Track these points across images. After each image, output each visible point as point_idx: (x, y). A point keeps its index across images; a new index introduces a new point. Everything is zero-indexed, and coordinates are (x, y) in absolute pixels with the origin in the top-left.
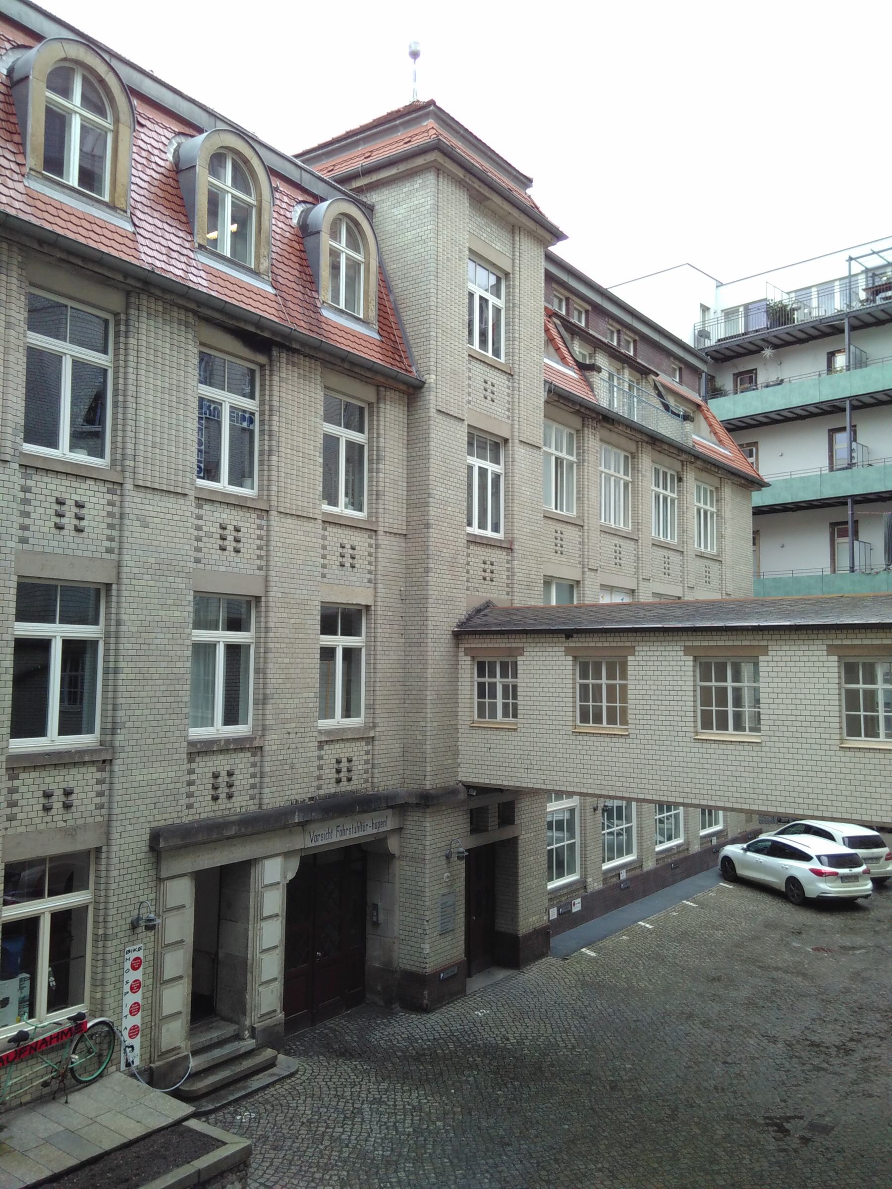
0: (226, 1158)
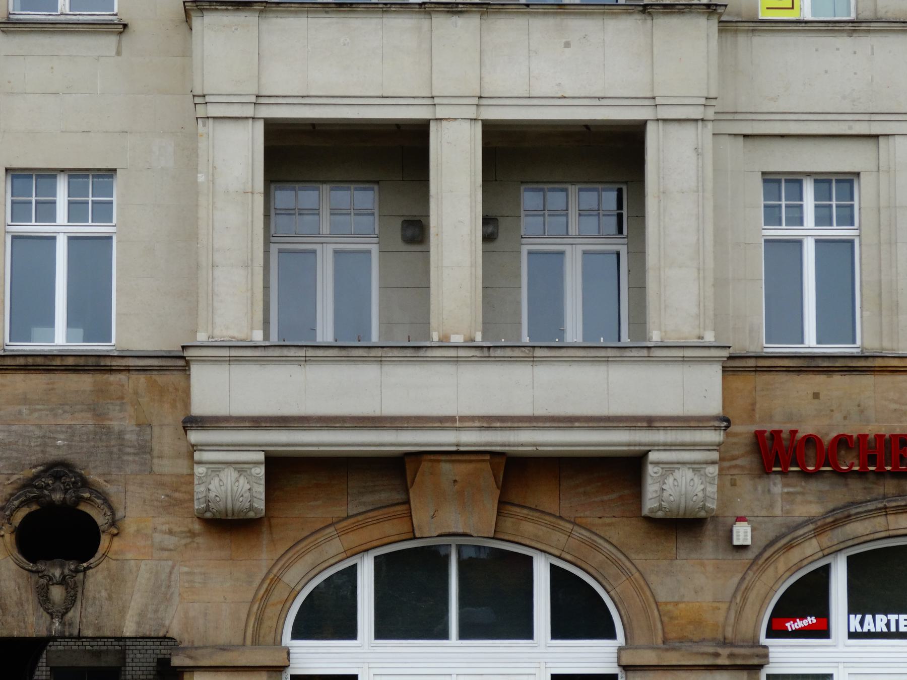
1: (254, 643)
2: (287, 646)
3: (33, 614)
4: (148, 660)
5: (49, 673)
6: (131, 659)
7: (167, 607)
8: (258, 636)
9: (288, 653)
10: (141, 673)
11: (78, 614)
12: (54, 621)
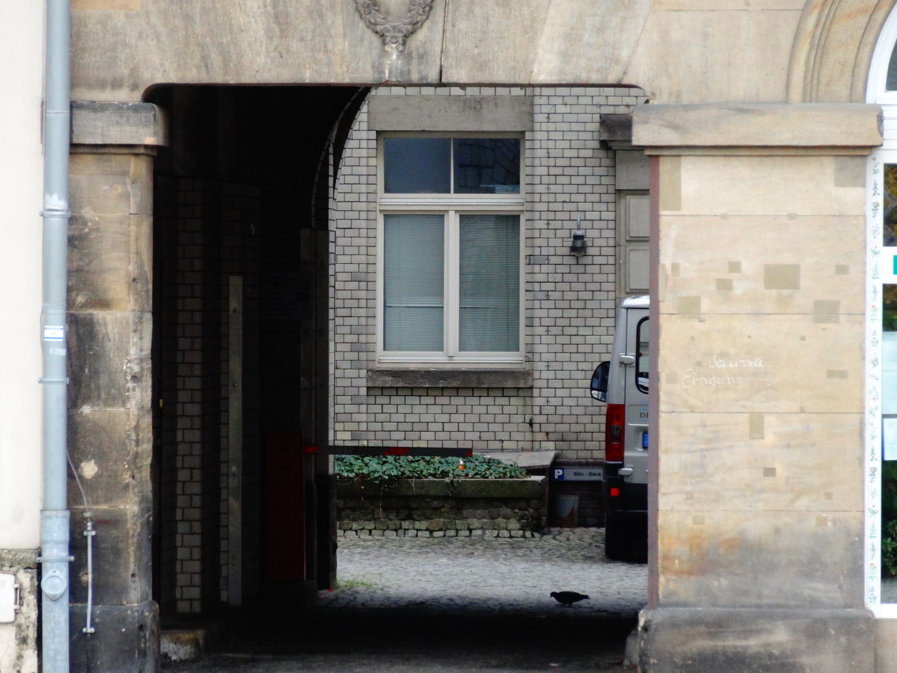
1: (808, 99)
2: (878, 102)
3: (344, 35)
4: (582, 118)
5: (373, 144)
6: (547, 115)
7: (624, 20)
8: (815, 82)
9: (880, 119)
11: (438, 37)
12: (387, 48)
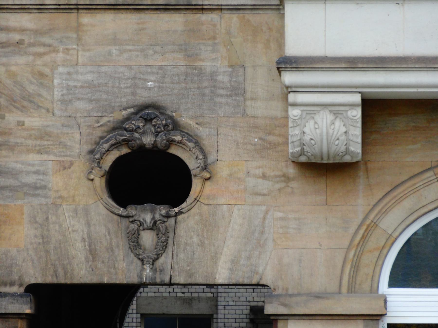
0: (394, 92)
10: (233, 320)
